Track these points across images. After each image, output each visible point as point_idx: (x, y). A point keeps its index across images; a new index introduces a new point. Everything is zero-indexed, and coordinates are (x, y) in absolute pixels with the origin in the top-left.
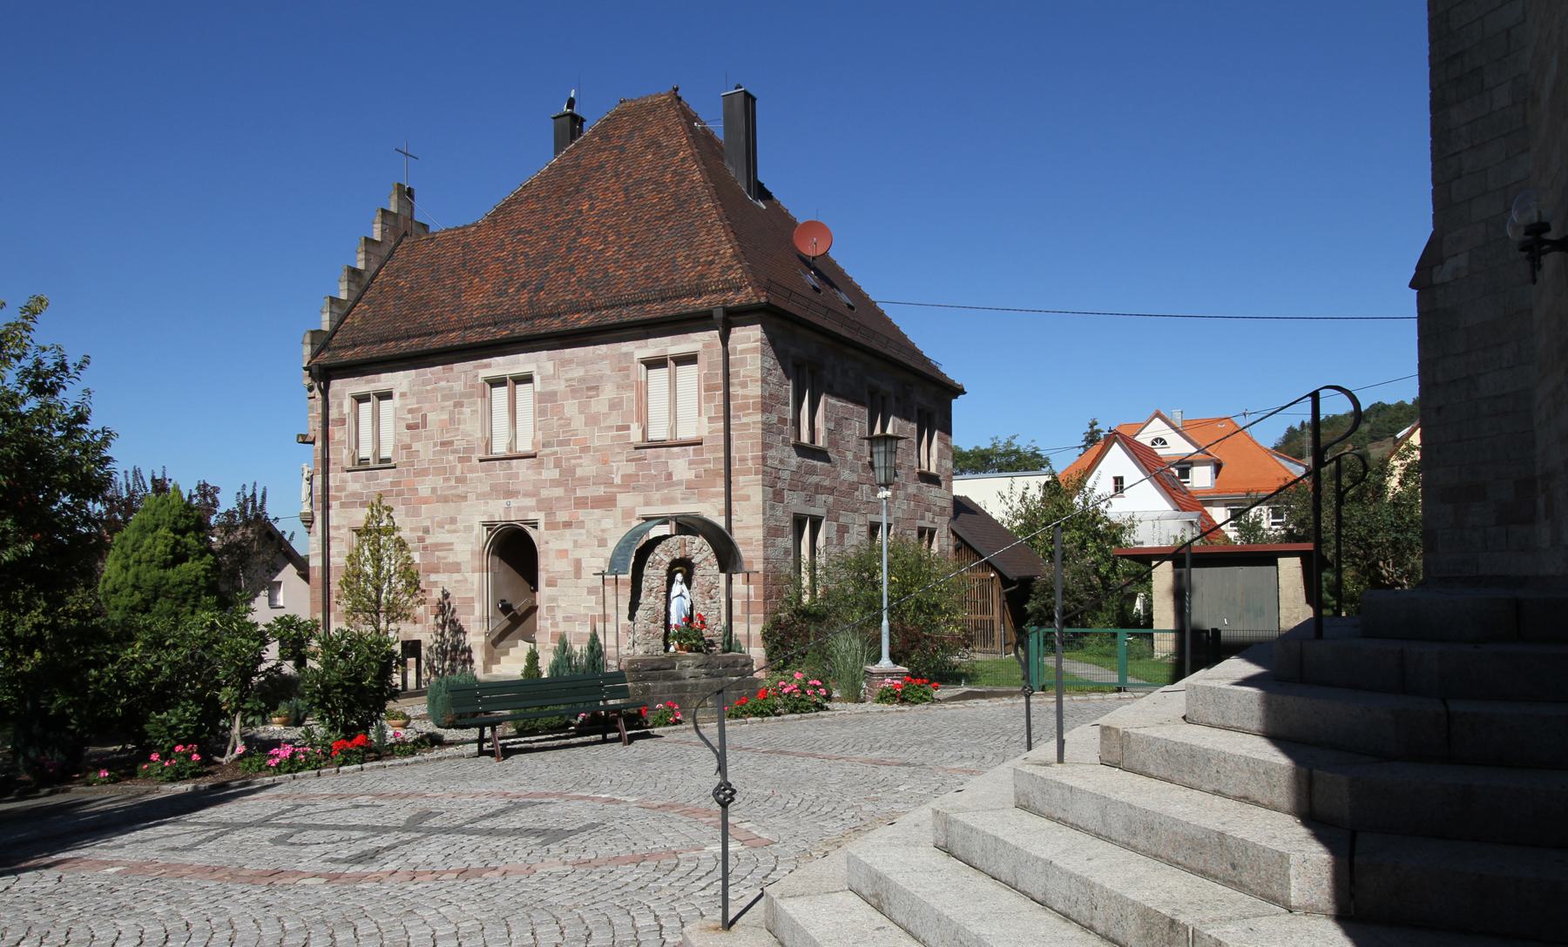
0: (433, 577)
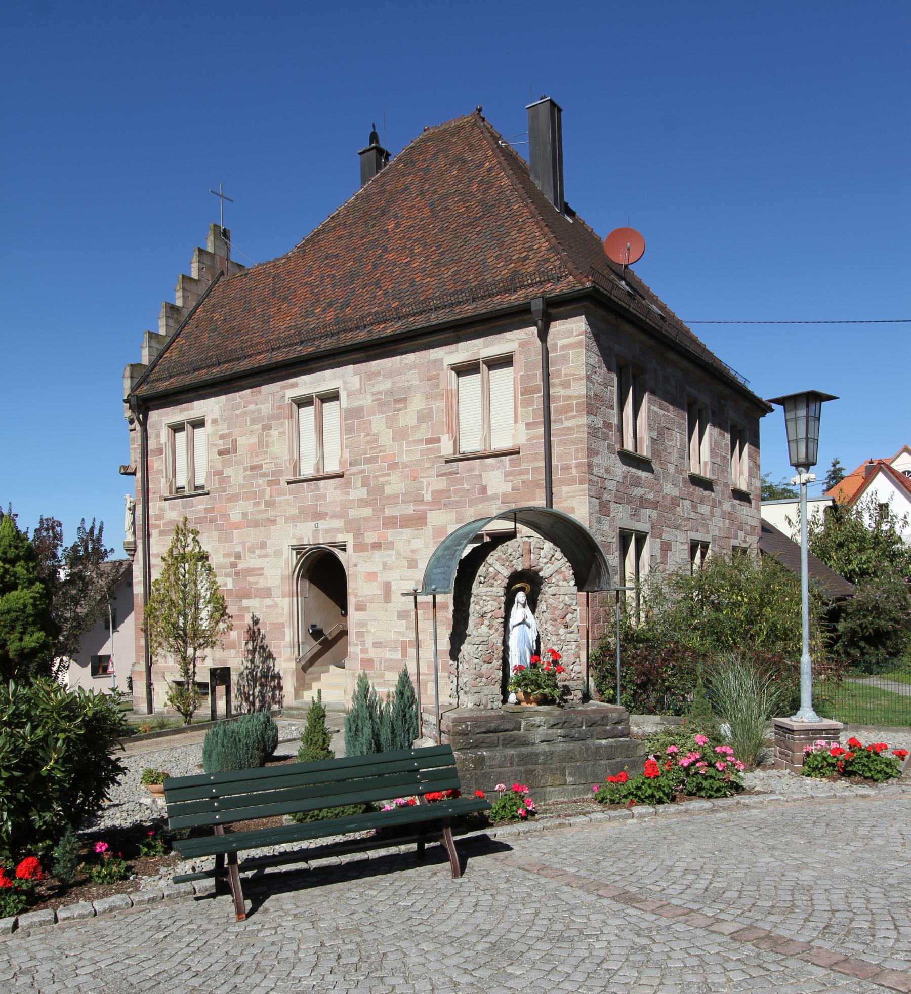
0: (245, 603)
